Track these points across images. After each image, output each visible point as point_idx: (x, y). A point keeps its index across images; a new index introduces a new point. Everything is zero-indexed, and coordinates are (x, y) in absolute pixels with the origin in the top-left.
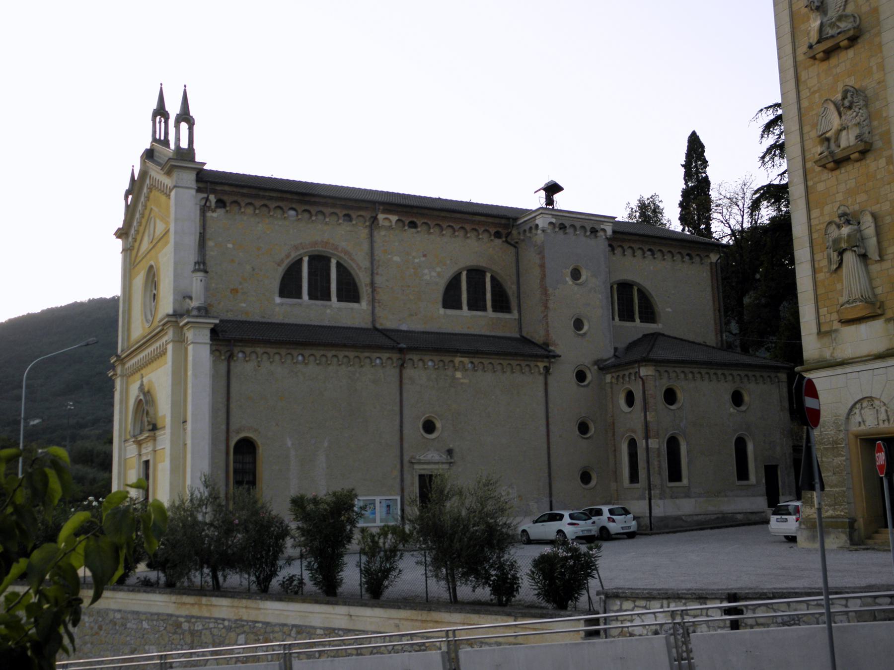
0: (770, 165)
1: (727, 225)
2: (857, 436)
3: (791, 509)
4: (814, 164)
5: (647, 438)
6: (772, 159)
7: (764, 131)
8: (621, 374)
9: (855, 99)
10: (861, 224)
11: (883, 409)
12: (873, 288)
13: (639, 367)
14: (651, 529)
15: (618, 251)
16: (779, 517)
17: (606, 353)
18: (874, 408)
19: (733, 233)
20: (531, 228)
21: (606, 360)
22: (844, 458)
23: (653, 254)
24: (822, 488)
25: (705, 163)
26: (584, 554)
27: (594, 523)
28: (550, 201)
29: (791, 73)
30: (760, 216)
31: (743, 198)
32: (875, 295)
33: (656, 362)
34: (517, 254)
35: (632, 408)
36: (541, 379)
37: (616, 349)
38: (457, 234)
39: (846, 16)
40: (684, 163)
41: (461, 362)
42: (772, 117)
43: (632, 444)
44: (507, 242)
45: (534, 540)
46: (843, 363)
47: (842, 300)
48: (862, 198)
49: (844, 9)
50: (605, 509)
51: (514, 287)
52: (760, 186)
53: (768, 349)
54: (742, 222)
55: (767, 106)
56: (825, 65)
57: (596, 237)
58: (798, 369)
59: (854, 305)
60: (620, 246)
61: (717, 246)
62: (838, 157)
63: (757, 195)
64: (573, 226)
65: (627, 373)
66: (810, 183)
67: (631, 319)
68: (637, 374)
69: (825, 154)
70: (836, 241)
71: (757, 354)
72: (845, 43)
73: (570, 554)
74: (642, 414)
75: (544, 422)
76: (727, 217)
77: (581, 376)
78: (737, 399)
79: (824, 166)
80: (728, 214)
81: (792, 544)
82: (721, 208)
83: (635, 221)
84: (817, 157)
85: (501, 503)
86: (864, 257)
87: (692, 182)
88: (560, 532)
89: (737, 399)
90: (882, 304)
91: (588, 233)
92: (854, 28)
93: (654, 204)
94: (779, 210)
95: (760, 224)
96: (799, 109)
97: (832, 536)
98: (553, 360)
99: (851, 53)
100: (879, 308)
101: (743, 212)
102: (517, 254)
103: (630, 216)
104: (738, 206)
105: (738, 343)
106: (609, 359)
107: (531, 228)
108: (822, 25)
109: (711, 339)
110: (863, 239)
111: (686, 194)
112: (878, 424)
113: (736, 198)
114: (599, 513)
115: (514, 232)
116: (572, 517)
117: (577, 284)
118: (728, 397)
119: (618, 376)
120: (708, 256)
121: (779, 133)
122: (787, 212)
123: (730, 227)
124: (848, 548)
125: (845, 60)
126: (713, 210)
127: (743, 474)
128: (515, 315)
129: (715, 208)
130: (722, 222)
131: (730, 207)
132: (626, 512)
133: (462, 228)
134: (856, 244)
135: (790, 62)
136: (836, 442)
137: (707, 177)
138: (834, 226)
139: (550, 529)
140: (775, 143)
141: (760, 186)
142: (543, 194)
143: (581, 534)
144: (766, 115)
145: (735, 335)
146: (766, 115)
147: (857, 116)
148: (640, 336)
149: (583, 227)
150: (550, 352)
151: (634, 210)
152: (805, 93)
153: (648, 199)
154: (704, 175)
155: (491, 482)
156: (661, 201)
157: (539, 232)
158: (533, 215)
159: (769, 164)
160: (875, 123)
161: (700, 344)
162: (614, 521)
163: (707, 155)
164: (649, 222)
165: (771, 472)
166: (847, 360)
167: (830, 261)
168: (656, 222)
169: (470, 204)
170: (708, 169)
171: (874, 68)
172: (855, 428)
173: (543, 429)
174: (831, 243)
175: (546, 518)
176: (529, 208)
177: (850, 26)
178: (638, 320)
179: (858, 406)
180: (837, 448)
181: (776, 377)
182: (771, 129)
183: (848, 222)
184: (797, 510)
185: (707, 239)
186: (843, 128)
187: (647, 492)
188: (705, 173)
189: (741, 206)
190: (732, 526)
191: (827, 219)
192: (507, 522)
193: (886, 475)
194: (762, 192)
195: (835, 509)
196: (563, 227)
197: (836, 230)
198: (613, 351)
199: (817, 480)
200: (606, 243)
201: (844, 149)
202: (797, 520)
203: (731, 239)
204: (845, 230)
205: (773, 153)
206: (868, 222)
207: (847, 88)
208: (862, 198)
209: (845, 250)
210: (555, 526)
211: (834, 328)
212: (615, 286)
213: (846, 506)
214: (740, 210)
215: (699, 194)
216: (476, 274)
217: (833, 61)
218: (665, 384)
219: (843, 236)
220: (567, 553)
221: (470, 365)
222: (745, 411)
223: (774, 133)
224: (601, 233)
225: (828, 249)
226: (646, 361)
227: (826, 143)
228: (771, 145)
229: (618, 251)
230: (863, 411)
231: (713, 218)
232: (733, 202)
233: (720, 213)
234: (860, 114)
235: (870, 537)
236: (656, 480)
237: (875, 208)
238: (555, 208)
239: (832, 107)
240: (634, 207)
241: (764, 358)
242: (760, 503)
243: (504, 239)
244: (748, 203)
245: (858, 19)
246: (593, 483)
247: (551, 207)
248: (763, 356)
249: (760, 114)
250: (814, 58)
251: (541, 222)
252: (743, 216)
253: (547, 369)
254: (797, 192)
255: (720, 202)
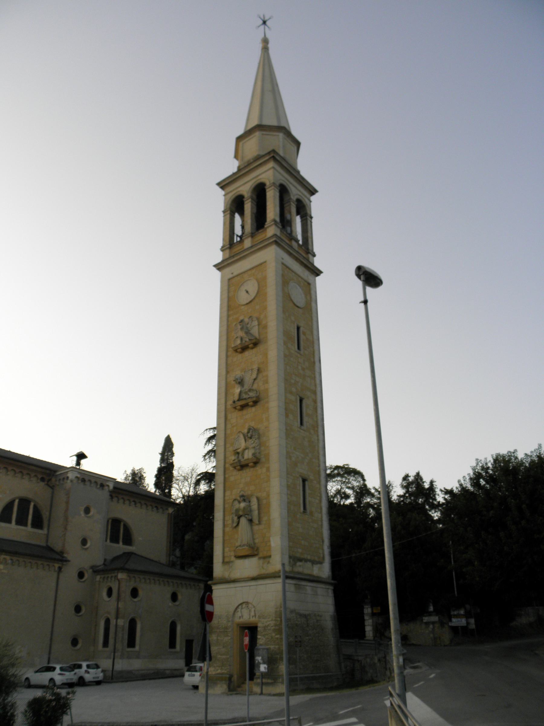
0: (208, 461)
1: (180, 492)
2: (238, 625)
3: (198, 668)
4: (230, 466)
5: (117, 618)
6: (210, 457)
7: (207, 441)
8: (106, 576)
9: (254, 434)
10: (251, 502)
11: (253, 610)
12: (254, 539)
13: (118, 573)
14: (112, 679)
15: (115, 499)
16: (190, 673)
17: (99, 562)
18: (248, 609)
19: (184, 497)
20: (64, 479)
21: (99, 566)
22: (230, 638)
23: (135, 504)
24: (210, 659)
25: (173, 454)
26: (64, 698)
27: (75, 674)
28: (78, 463)
29: (223, 414)
30: (199, 489)
31: (191, 477)
32: (255, 544)
33: (129, 571)
34: (53, 493)
35: (110, 599)
36: (55, 575)
37: (105, 560)
38: (16, 475)
39: (253, 390)
40: (161, 452)
41: (4, 558)
42: (212, 434)
43: (108, 621)
44: (47, 485)
45: (33, 685)
46: (234, 581)
47: (238, 544)
48: (252, 488)
49: (252, 386)
50: (84, 664)
51: (48, 513)
52: (201, 472)
53: (196, 568)
54: (189, 491)
55: (210, 428)
56: (240, 413)
57: (103, 489)
58: (210, 582)
59: (243, 548)
60: (117, 497)
61: (174, 504)
62: (243, 463)
63: (199, 477)
64: (90, 481)
65: (110, 576)
66: (227, 476)
67: (117, 542)
68: (116, 577)
69: (236, 461)
70: (237, 510)
71: (189, 570)
72: (251, 404)
73: (54, 698)
74: (116, 603)
75: (52, 603)
76: (181, 487)
77: (81, 575)
78: (174, 597)
79: (235, 468)
80: (182, 486)
81: (196, 691)
82: (178, 482)
83: (128, 482)
84: (232, 462)
85: (13, 659)
86: (251, 521)
87: (164, 464)
88: (52, 680)
89: (174, 597)
90: (258, 549)
91: (98, 486)
92: (256, 397)
93: (141, 474)
94: (210, 487)
95: (199, 493)
96: (225, 434)
97: (219, 686)
98: (64, 563)
99: (253, 409)
100: (256, 551)
101: (190, 485)
102: (53, 493)
103: (126, 479)
104: (188, 482)
105: (179, 563)
106: (100, 566)
107: (64, 479)
108: (241, 392)
109: (163, 559)
110: (251, 511)
111: (160, 470)
112: (250, 618)
113: (187, 477)
114: (80, 667)
115: (53, 479)
116: (61, 669)
117: (87, 517)
118: (169, 596)
119: (104, 577)
120: (167, 509)
121: (214, 444)
122: (214, 489)
123: (182, 493)
124: (227, 693)
125: (250, 412)
126: (174, 482)
127: (172, 644)
128: (45, 531)
129: (175, 481)
130: (178, 490)
131: (183, 481)
132: (97, 667)
133: (21, 472)
134: (247, 513)
135: (223, 408)
136: (226, 628)
137: (172, 463)
138: (236, 502)
139: (44, 678)
140: (212, 449)
141: (201, 472)
142: (75, 458)
143: (65, 681)
144: (209, 433)
145: (178, 558)
146: (209, 433)
147: (254, 443)
148: (121, 553)
149: (96, 482)
150: (63, 557)
151: (128, 476)
152: (229, 426)
153: (137, 470)
154: (171, 461)
155: (9, 644)
156: (145, 473)
157: (69, 481)
158: (67, 470)
159: (208, 461)
160: (262, 448)
161: (156, 562)
162: (88, 673)
163: (175, 449)
164: (136, 484)
165: (189, 644)
166: (239, 579)
167: (233, 522)
168: (140, 484)
169: (28, 458)
170: (174, 458)
171: (264, 419)
172: (237, 620)
173: (52, 608)
174: (234, 511)
175: (44, 669)
176: (65, 466)
177: (254, 395)
178: (121, 543)
179: (240, 607)
180: (226, 631)
181: (198, 585)
182: (211, 441)
183: (244, 500)
184: (201, 669)
185: (168, 499)
186: (246, 448)
187: (112, 654)
188: (172, 459)
189: (190, 482)
190: (162, 678)
191: (234, 497)
192: (15, 673)
193: (249, 650)
194: (202, 475)
195: (222, 669)
196: (83, 480)
197: (238, 504)
198: (103, 561)
199: (208, 655)
200: (108, 494)
201: (246, 460)
202: (200, 675)
203: (182, 500)
204: (243, 505)
205: (210, 454)
206: (254, 502)
207: (250, 427)
208: (252, 488)
209: (241, 516)
210: (48, 675)
211: (232, 560)
212: (110, 521)
213: (228, 667)
214: (189, 484)
215: (167, 472)
216: (24, 502)
217: (245, 412)
218: (132, 584)
219: (241, 508)
220: (52, 696)
221: (10, 561)
222: (177, 606)
223: (212, 443)
224: (106, 488)
225: (233, 515)
226: (122, 569)
227: (237, 455)
228: (210, 450)
229: (115, 499)
230: (243, 610)
231: (173, 487)
232: (186, 479)
233: (177, 484)
234: (255, 442)
235: (239, 686)
236: (119, 646)
237: (259, 495)
238: (81, 468)
239: (242, 436)
240: (129, 474)
241: (192, 573)
242: (180, 663)
243: (46, 483)
244: (194, 480)
245: (258, 392)
246: (79, 646)
247: (78, 467)
248: (193, 571)
249: (206, 432)
250: (235, 408)
251: (71, 476)
252: (190, 488)
253: (60, 569)
254: (219, 479)
255: (178, 478)
